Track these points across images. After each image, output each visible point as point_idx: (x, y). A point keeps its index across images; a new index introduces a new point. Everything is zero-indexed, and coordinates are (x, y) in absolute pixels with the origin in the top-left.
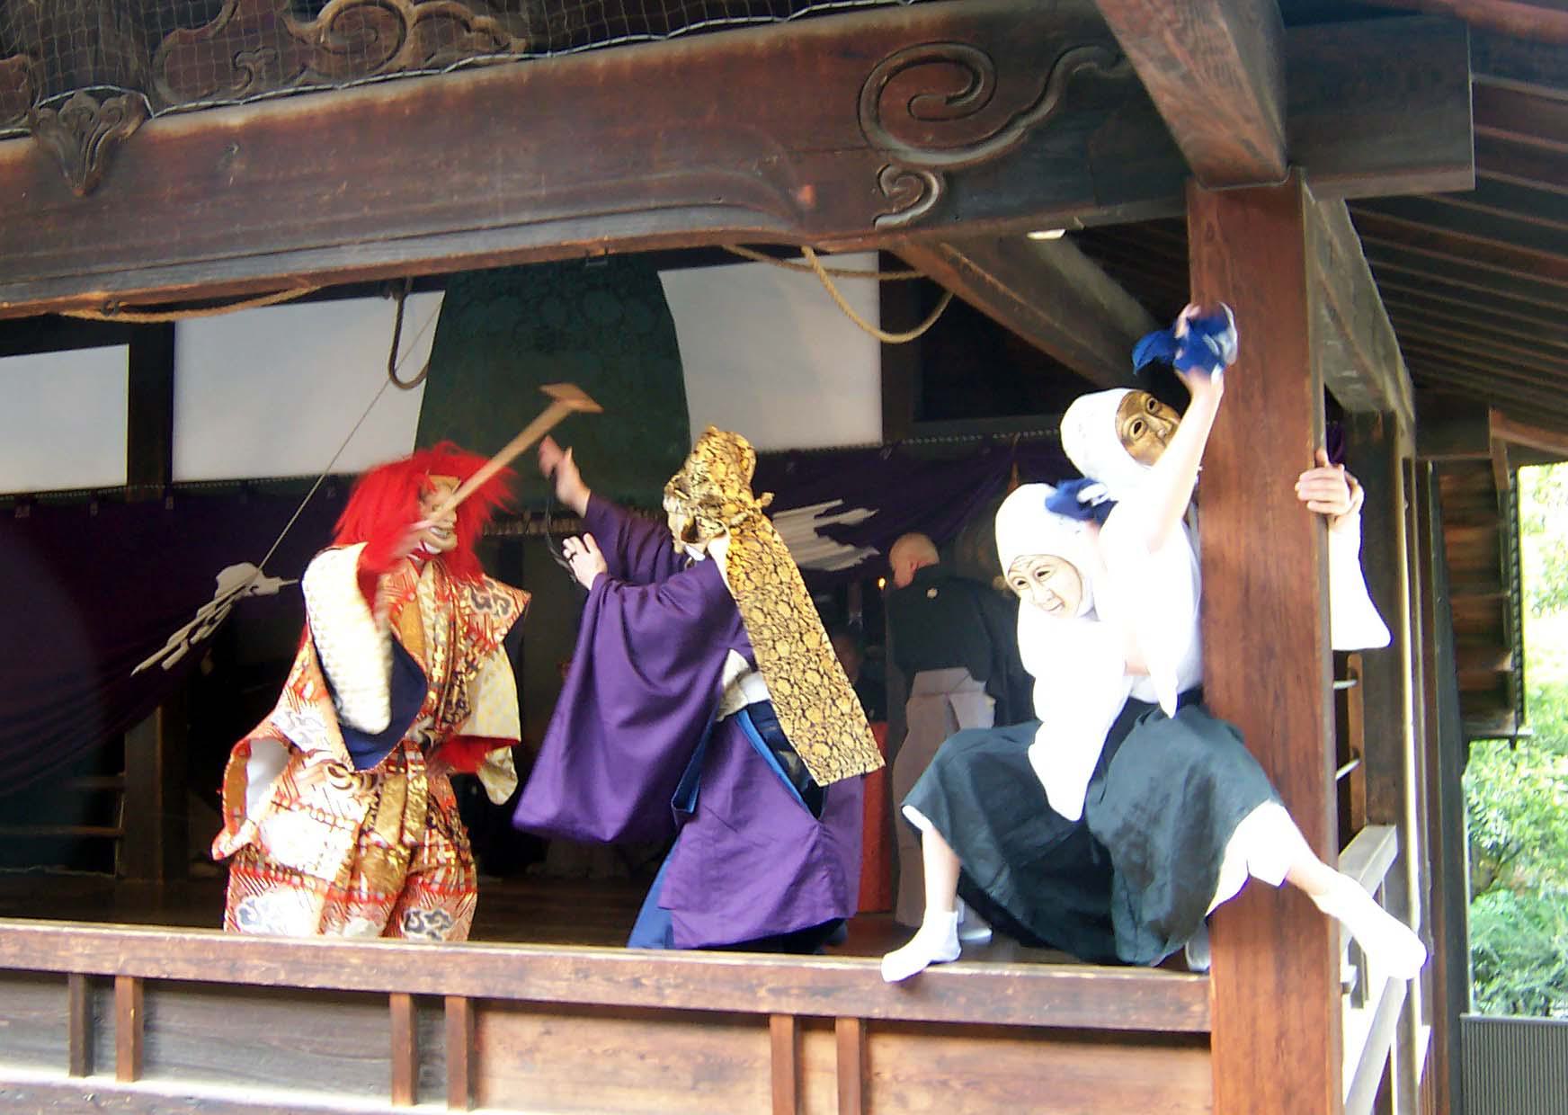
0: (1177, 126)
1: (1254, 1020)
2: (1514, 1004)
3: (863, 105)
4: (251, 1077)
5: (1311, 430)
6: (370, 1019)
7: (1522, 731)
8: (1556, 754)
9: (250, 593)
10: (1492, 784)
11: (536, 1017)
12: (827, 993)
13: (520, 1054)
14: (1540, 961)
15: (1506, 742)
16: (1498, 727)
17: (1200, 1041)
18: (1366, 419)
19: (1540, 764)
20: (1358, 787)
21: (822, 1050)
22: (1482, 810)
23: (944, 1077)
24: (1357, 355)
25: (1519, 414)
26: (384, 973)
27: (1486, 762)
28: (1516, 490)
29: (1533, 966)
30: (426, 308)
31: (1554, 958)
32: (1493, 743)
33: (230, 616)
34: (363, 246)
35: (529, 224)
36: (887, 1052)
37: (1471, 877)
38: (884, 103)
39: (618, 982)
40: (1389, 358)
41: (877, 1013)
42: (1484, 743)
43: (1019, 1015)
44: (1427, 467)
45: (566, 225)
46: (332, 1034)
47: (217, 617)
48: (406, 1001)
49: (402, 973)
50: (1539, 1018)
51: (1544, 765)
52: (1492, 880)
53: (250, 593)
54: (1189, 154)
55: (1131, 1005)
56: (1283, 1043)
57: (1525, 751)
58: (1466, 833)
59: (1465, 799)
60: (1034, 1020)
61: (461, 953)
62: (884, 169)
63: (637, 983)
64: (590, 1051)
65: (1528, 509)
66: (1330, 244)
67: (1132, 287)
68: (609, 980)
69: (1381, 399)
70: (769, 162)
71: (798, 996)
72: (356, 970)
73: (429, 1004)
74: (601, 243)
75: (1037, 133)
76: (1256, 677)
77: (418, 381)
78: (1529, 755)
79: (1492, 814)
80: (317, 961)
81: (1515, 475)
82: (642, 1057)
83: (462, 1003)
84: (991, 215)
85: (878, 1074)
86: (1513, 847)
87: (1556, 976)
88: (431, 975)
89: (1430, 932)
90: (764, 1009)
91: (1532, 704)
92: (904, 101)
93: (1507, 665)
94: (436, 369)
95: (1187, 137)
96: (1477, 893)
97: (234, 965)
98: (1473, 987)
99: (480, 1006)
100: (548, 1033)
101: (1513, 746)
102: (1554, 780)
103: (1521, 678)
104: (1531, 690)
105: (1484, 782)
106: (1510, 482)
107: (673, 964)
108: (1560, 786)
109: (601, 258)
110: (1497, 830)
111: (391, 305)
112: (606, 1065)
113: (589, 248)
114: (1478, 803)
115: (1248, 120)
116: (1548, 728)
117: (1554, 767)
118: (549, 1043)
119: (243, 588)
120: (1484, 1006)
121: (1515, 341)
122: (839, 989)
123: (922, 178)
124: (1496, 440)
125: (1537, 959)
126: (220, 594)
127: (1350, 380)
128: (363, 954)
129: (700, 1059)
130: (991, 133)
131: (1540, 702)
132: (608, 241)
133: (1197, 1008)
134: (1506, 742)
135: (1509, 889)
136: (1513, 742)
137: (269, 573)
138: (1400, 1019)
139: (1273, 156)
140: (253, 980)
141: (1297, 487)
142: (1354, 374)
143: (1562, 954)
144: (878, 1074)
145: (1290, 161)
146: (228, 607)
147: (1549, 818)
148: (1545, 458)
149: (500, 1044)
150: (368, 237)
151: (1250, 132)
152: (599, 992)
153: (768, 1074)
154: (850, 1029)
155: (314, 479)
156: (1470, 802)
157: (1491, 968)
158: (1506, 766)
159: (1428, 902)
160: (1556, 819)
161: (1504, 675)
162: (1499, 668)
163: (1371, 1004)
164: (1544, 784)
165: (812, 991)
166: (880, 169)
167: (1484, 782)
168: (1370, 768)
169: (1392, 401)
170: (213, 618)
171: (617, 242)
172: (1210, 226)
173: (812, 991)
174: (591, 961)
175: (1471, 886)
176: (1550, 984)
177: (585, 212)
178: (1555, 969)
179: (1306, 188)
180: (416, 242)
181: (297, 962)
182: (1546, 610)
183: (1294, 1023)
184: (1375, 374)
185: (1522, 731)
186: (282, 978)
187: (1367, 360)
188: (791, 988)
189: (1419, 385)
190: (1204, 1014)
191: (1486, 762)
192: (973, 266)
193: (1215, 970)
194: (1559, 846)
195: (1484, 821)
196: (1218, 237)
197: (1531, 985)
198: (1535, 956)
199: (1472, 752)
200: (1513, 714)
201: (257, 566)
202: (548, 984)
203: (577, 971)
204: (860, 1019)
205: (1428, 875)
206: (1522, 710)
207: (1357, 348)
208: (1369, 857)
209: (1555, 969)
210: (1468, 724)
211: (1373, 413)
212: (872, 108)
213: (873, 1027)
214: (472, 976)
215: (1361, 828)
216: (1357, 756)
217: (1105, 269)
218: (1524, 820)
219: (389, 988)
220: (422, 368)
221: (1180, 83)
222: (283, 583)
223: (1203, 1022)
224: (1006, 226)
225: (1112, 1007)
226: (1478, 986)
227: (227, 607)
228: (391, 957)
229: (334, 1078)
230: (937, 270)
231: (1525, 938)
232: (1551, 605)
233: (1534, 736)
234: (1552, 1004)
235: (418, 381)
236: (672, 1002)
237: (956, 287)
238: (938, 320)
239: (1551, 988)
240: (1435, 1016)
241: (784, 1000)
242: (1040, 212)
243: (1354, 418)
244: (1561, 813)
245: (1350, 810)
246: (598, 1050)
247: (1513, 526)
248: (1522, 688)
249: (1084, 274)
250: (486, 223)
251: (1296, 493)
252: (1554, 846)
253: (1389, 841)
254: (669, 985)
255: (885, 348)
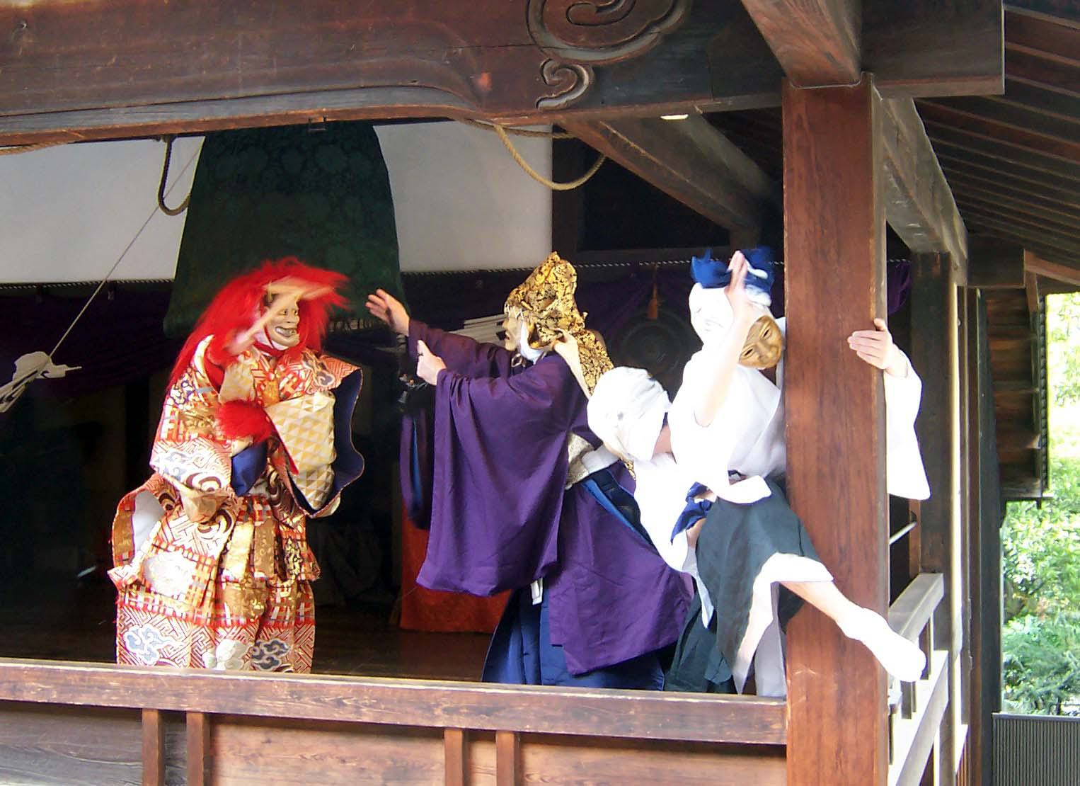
0: (772, 41)
1: (820, 736)
2: (1036, 703)
3: (530, 11)
4: (28, 777)
5: (873, 280)
6: (127, 730)
7: (1045, 495)
8: (1072, 512)
9: (42, 377)
10: (1023, 536)
11: (260, 729)
12: (489, 712)
13: (246, 758)
14: (1055, 670)
15: (1035, 502)
16: (1028, 491)
17: (778, 752)
18: (927, 258)
19: (1059, 520)
20: (915, 544)
21: (485, 757)
22: (1015, 555)
23: (579, 778)
24: (919, 212)
25: (1044, 254)
26: (138, 693)
27: (1018, 518)
28: (1044, 311)
29: (1050, 674)
30: (189, 151)
31: (1066, 667)
32: (1024, 503)
33: (25, 392)
34: (128, 109)
35: (262, 96)
36: (536, 758)
37: (1005, 605)
38: (547, 9)
39: (324, 702)
40: (947, 213)
41: (528, 728)
42: (1018, 503)
43: (638, 732)
44: (975, 294)
45: (292, 98)
46: (95, 742)
47: (13, 396)
48: (155, 716)
49: (152, 694)
50: (1054, 715)
51: (1061, 520)
52: (1021, 608)
53: (42, 377)
54: (783, 62)
55: (725, 723)
56: (842, 753)
57: (1048, 510)
58: (1002, 572)
59: (1001, 547)
60: (650, 735)
61: (199, 678)
62: (545, 63)
63: (339, 703)
64: (302, 756)
65: (1053, 323)
66: (898, 129)
67: (748, 150)
68: (318, 700)
69: (940, 244)
70: (455, 53)
71: (467, 715)
72: (115, 691)
73: (173, 718)
74: (321, 113)
75: (669, 38)
76: (826, 470)
77: (181, 209)
78: (1051, 513)
79: (1022, 557)
80: (83, 683)
81: (1043, 300)
82: (344, 761)
83: (200, 718)
84: (629, 101)
85: (528, 776)
86: (1037, 583)
87: (1065, 682)
88: (175, 695)
89: (969, 652)
90: (440, 724)
91: (1055, 474)
92: (563, 9)
93: (1036, 445)
94: (196, 202)
95: (781, 49)
96: (1010, 617)
97: (15, 687)
98: (1006, 690)
99: (214, 720)
100: (269, 741)
101: (1039, 506)
102: (1069, 532)
103: (1046, 454)
104: (1054, 463)
105: (1016, 533)
106: (1040, 304)
107: (368, 688)
108: (1074, 536)
109: (319, 125)
110: (1025, 569)
111: (163, 145)
112: (314, 767)
113: (312, 117)
114: (1012, 550)
115: (828, 38)
116: (1067, 492)
117: (1070, 522)
118: (268, 749)
119: (36, 372)
120: (1013, 705)
121: (1038, 201)
122: (499, 709)
123: (576, 70)
124: (1029, 274)
125: (1053, 669)
126: (17, 377)
127: (914, 229)
128: (121, 678)
129: (389, 763)
130: (631, 37)
131: (1060, 472)
132: (326, 112)
133: (776, 726)
134: (1035, 502)
135: (1034, 614)
136: (1039, 502)
137: (57, 360)
138: (942, 722)
139: (850, 66)
140: (31, 699)
141: (849, 340)
142: (918, 226)
143: (1072, 665)
144: (528, 776)
145: (864, 68)
146: (23, 387)
147: (1067, 561)
148: (1070, 289)
149: (230, 750)
150: (132, 102)
151: (830, 47)
152: (309, 710)
153: (442, 775)
154: (507, 740)
155: (97, 284)
156: (1006, 547)
157: (1019, 674)
158: (1034, 520)
159: (969, 630)
160: (1070, 563)
161: (1033, 451)
162: (1029, 447)
163: (917, 716)
164: (1061, 535)
165: (476, 711)
166: (543, 63)
167: (1016, 533)
168: (924, 528)
169: (948, 245)
170: (10, 396)
171: (333, 113)
172: (800, 117)
173: (476, 711)
174: (303, 685)
175: (1005, 611)
176: (1062, 688)
177: (308, 88)
178: (1065, 677)
179: (875, 89)
180: (173, 108)
181: (67, 684)
182: (1068, 400)
183: (850, 736)
184: (935, 226)
185: (1045, 495)
186: (54, 697)
187: (928, 216)
188: (462, 708)
189: (970, 230)
190: (781, 732)
191: (1018, 518)
192: (619, 135)
193: (791, 697)
194: (1072, 583)
195: (1016, 562)
196: (805, 125)
197: (1049, 688)
198: (1051, 666)
199: (1008, 509)
200: (1039, 482)
201: (48, 354)
202: (268, 703)
203: (292, 693)
204: (515, 733)
205: (969, 608)
206: (1046, 478)
207: (919, 207)
208: (919, 602)
209: (1065, 677)
210: (1005, 489)
211: (933, 253)
212: (537, 14)
213: (525, 739)
214: (207, 696)
215: (917, 575)
216: (914, 520)
217: (728, 136)
218: (1045, 563)
219: (141, 705)
220: (186, 197)
221: (775, 9)
222: (69, 369)
223: (780, 739)
224: (641, 111)
225: (712, 726)
226: (1009, 689)
227: (22, 387)
228: (142, 681)
229: (96, 777)
230: (592, 138)
231: (1045, 653)
232: (1071, 396)
233: (1056, 497)
234: (1063, 703)
235: (181, 209)
236: (367, 717)
237: (608, 151)
238: (597, 172)
239: (1063, 691)
240: (971, 716)
241: (455, 717)
242: (668, 97)
243: (919, 256)
244: (1074, 558)
245: (908, 561)
246: (308, 756)
247: (1042, 338)
248: (1046, 462)
249: (714, 142)
250: (228, 95)
251: (848, 344)
252: (1068, 583)
253: (937, 586)
254: (366, 705)
255: (555, 193)
